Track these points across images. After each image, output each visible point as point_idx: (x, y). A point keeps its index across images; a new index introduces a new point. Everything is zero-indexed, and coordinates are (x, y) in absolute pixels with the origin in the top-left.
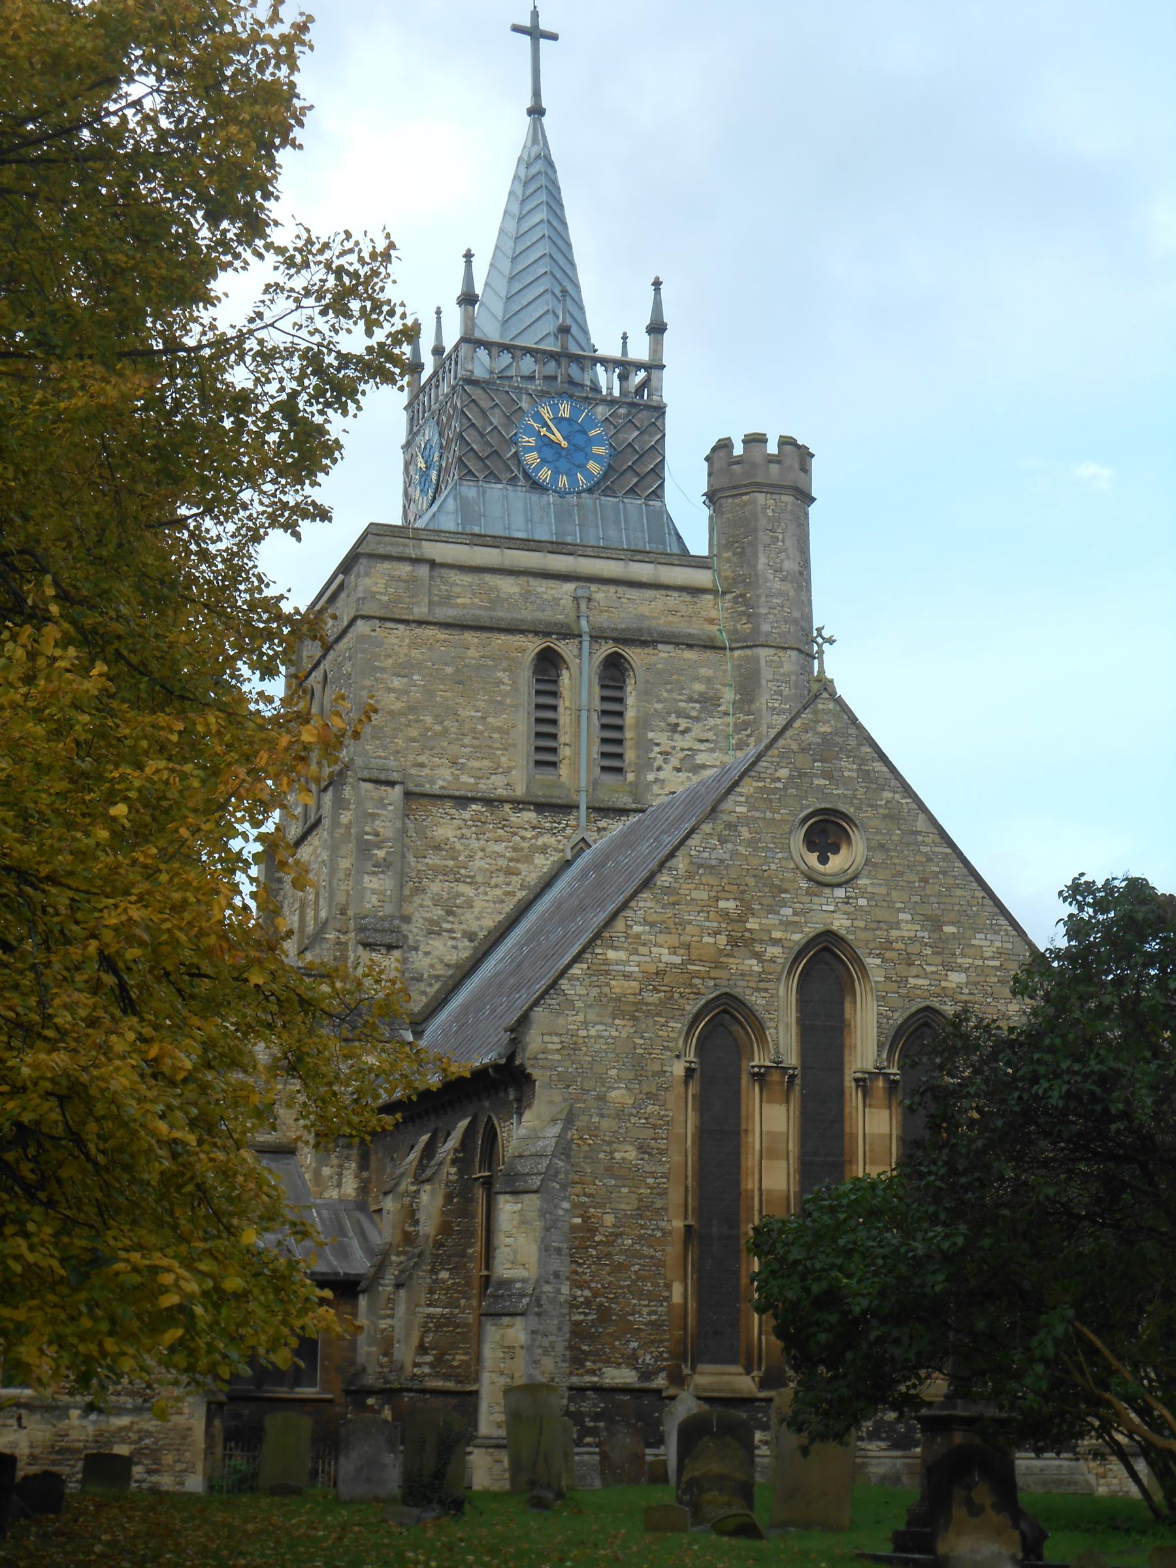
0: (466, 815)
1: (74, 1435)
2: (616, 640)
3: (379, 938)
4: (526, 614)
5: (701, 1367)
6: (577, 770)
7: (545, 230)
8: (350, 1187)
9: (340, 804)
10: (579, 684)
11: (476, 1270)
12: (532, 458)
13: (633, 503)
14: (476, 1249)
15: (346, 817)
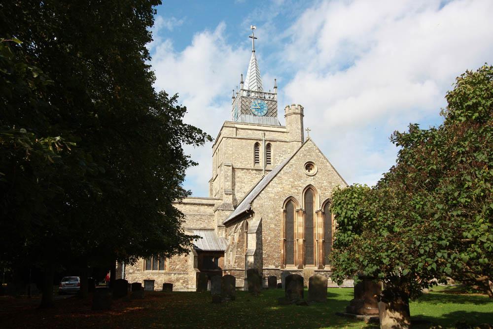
0: (243, 172)
1: (173, 278)
3: (228, 193)
4: (253, 137)
5: (287, 265)
6: (261, 164)
7: (255, 77)
8: (224, 235)
9: (221, 170)
10: (262, 149)
11: (245, 248)
12: (254, 110)
13: (272, 118)
14: (245, 244)
15: (222, 172)
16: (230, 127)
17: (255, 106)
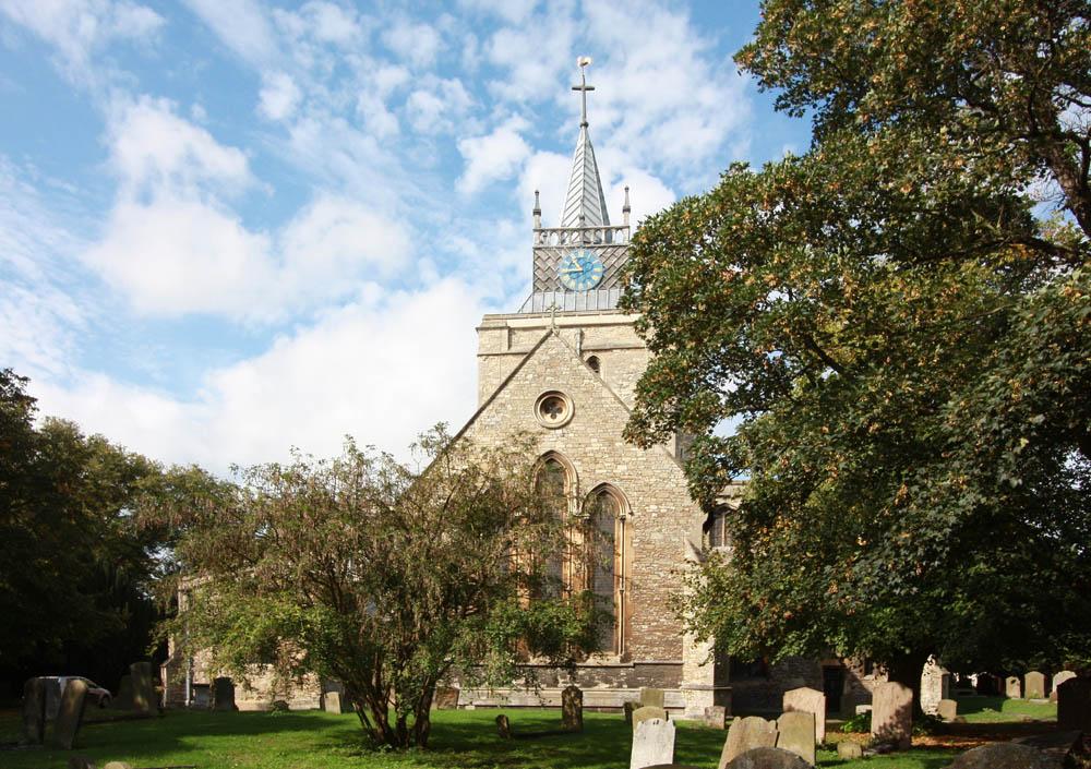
2: (593, 350)
16: (495, 328)
17: (570, 267)
